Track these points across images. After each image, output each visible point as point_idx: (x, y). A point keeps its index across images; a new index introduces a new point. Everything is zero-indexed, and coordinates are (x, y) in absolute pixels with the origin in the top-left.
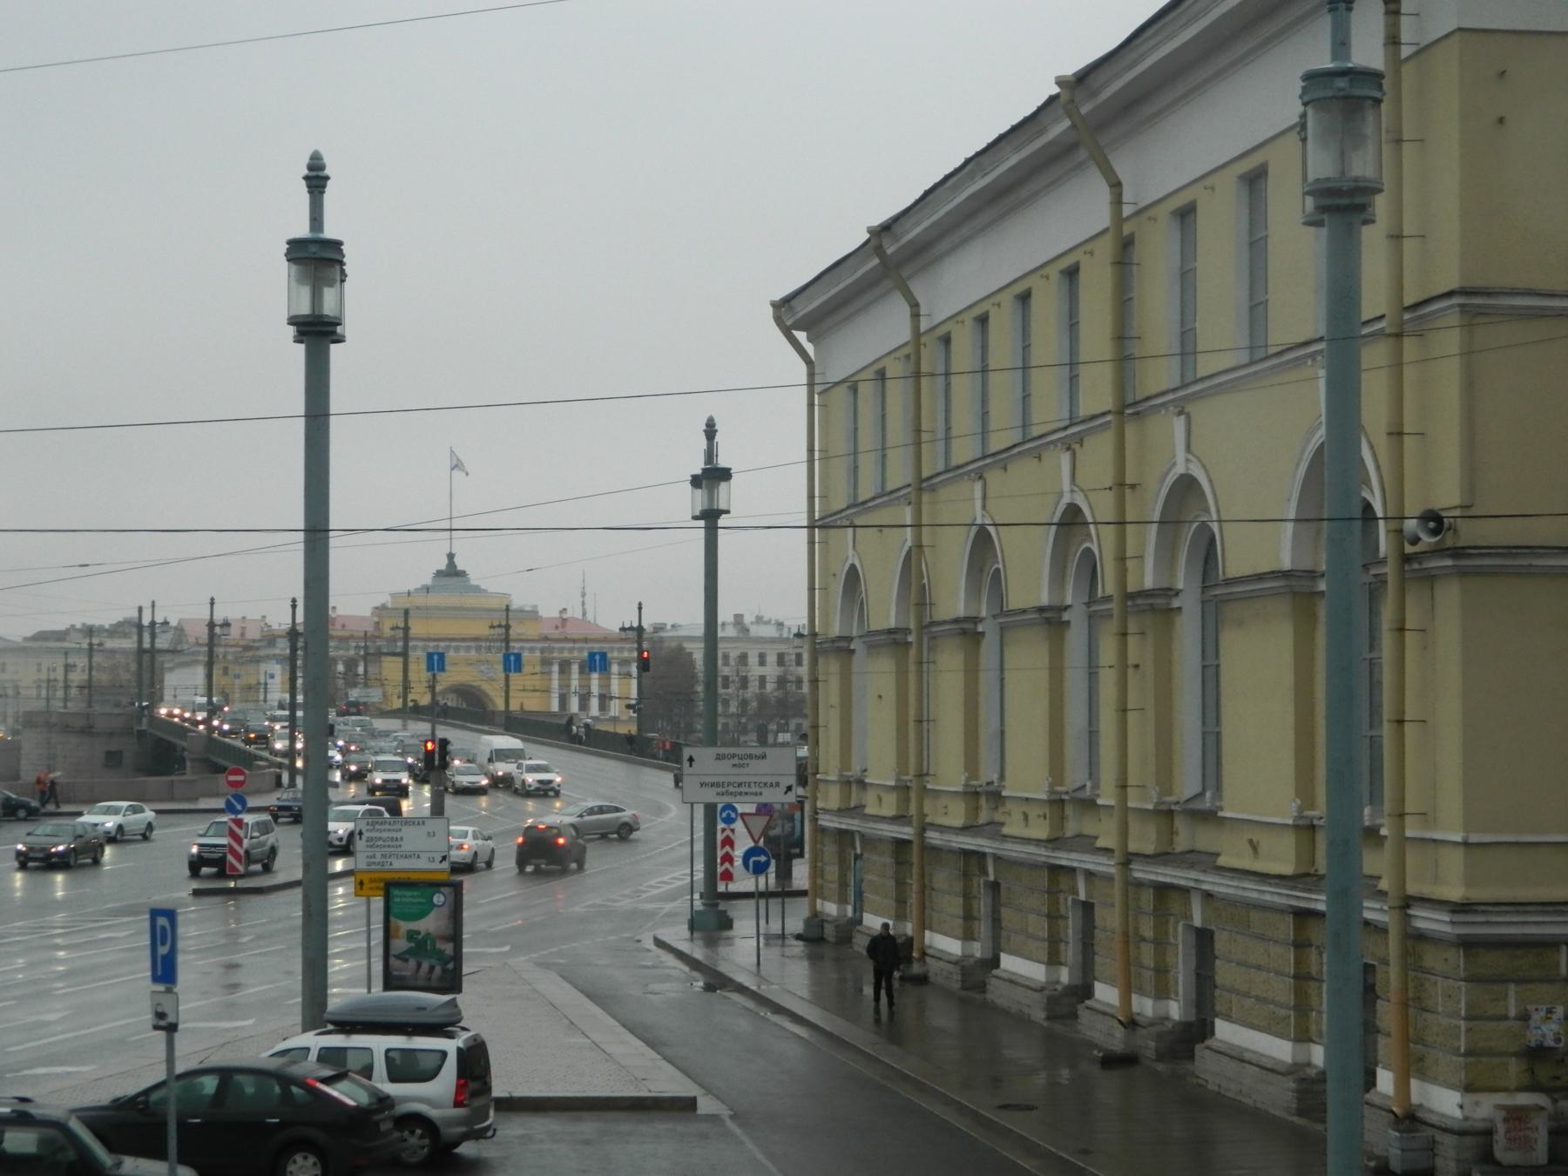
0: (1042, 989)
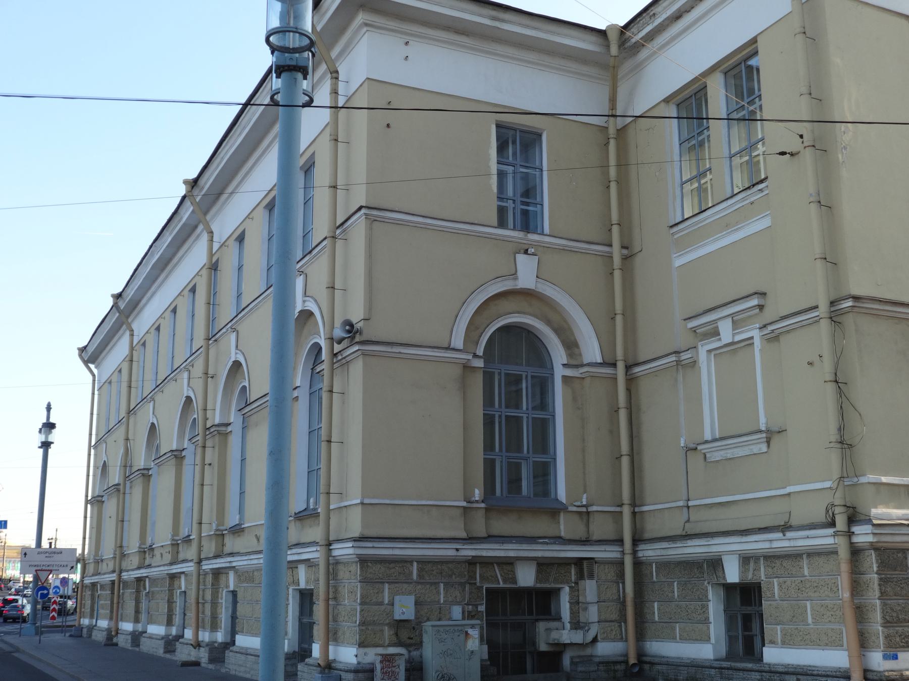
0: (163, 638)
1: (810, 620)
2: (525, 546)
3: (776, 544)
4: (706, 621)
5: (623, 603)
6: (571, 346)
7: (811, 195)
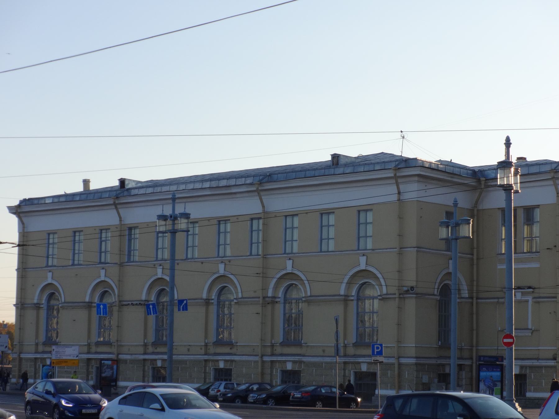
3: (534, 364)
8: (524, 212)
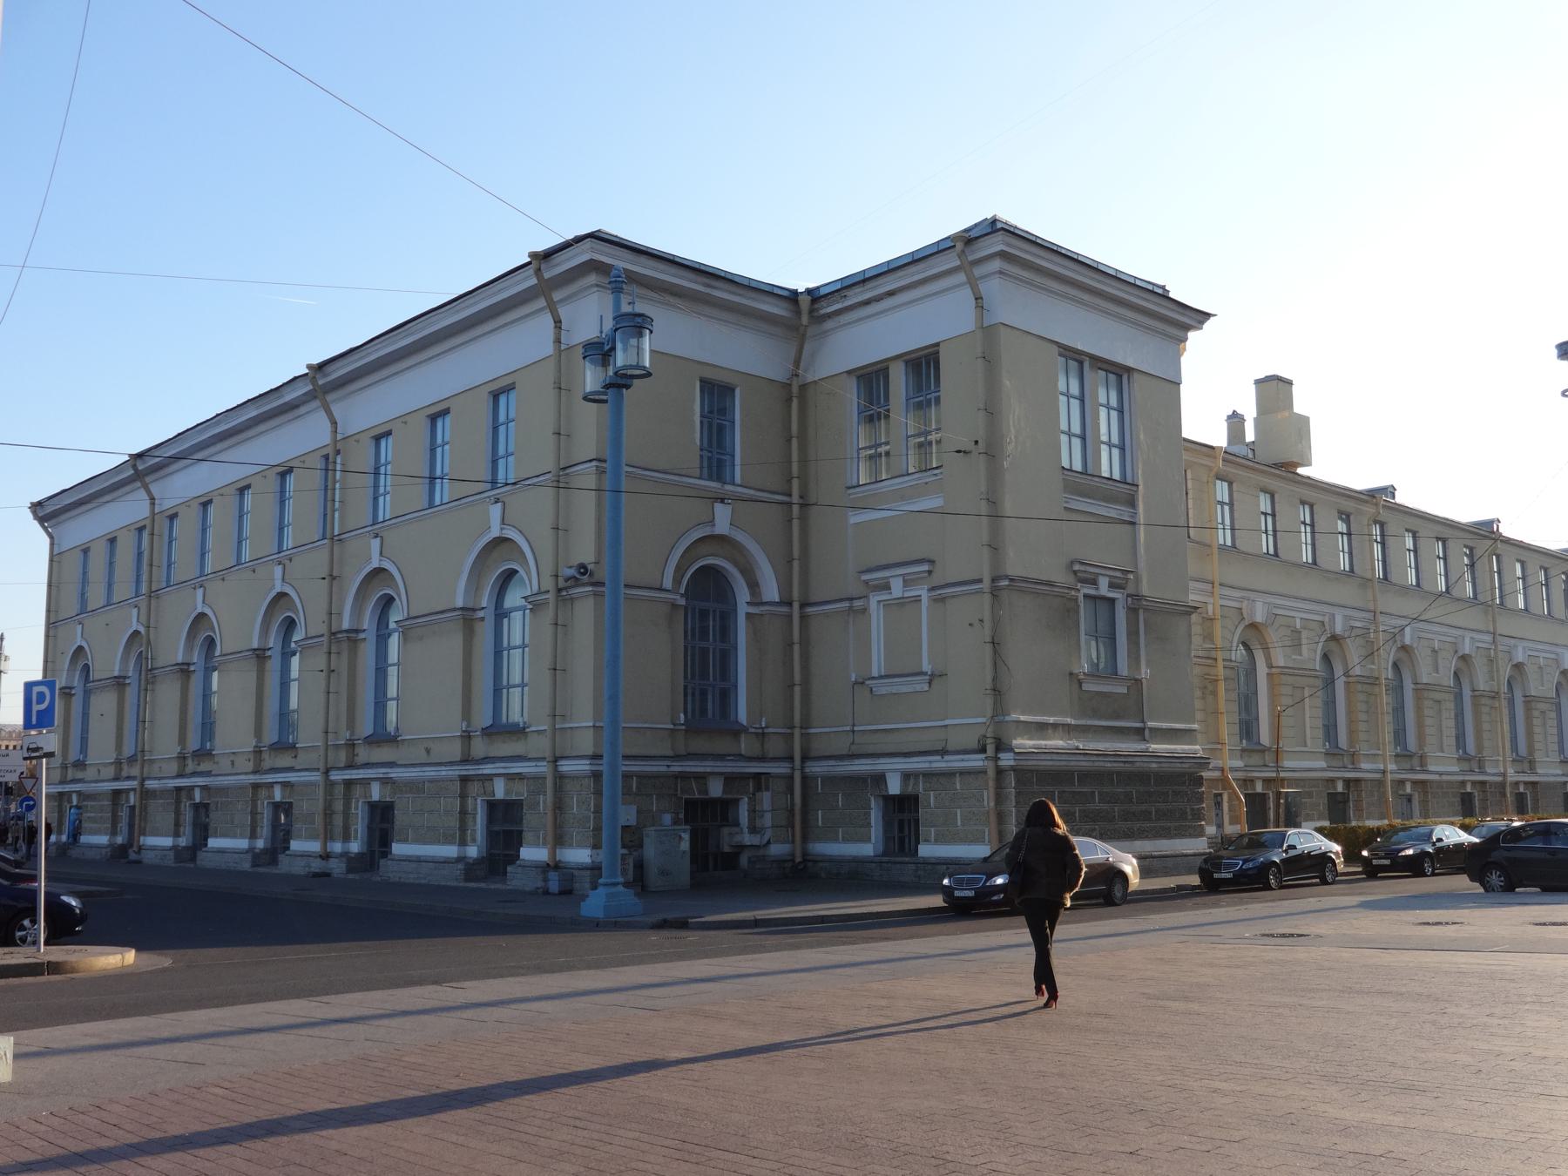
1: (959, 823)
2: (719, 764)
3: (934, 765)
4: (869, 825)
5: (791, 811)
6: (754, 586)
7: (982, 493)
8: (906, 374)
